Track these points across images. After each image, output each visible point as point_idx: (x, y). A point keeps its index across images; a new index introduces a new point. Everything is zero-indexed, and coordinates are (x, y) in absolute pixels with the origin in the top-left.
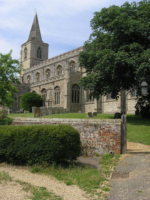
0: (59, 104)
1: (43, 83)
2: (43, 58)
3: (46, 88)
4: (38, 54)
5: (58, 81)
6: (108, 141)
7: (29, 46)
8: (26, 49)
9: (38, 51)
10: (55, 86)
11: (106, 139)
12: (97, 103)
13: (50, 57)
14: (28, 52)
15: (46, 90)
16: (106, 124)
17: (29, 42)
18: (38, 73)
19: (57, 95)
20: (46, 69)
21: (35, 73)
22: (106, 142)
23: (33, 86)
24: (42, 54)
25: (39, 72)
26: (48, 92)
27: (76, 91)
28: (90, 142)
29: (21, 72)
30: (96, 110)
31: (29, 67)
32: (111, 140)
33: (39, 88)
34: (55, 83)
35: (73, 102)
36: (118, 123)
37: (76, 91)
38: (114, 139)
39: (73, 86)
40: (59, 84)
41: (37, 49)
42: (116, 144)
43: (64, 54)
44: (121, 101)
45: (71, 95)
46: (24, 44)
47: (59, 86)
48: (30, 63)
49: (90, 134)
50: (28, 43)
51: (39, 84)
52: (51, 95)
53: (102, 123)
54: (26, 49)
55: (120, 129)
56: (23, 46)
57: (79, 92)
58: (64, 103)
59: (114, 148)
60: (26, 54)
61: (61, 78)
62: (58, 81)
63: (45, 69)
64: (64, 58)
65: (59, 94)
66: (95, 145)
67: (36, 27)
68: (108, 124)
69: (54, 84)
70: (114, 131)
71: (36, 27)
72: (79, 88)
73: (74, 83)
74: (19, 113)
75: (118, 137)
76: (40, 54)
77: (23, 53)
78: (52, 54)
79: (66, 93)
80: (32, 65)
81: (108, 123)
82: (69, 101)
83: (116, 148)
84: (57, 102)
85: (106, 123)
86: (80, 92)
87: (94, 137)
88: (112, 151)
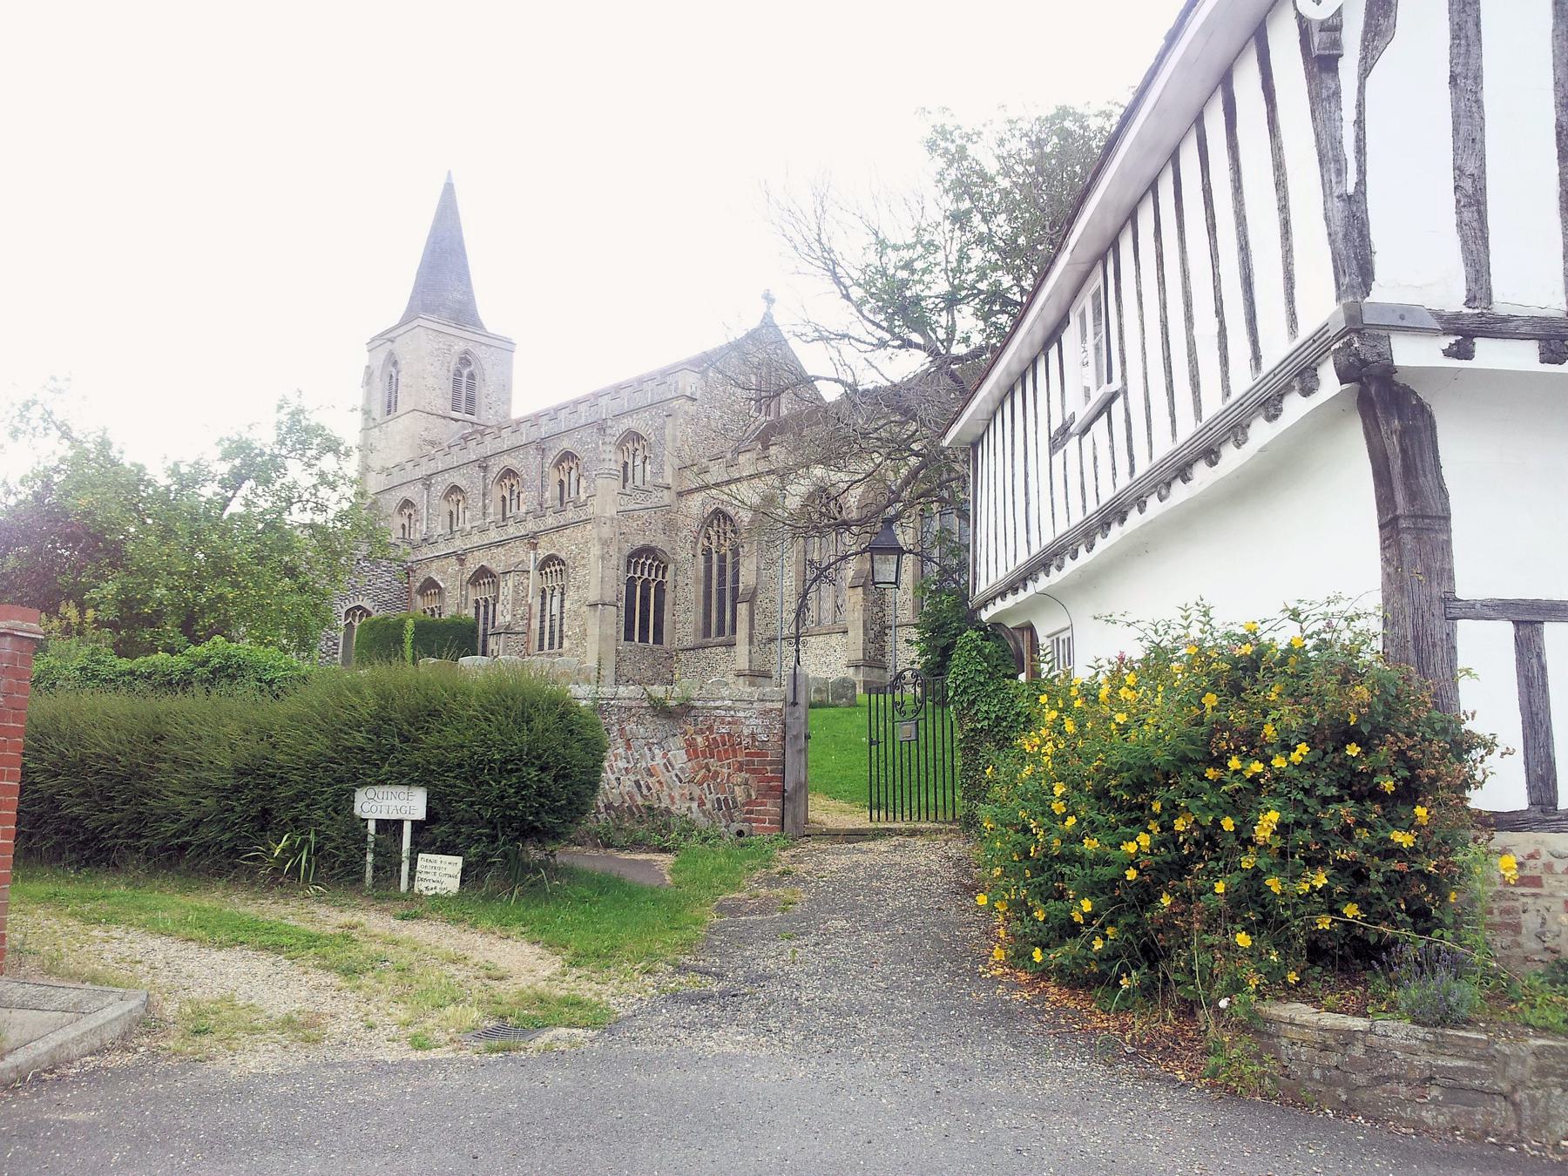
1: (476, 540)
3: (497, 568)
5: (559, 528)
9: (458, 373)
10: (542, 553)
11: (717, 773)
12: (751, 642)
15: (492, 575)
20: (496, 470)
21: (439, 488)
22: (720, 788)
24: (481, 393)
25: (462, 483)
26: (502, 584)
28: (649, 789)
29: (969, 220)
32: (739, 777)
35: (629, 637)
36: (769, 705)
38: (754, 771)
39: (631, 556)
40: (563, 545)
45: (622, 604)
47: (563, 555)
51: (458, 544)
54: (395, 363)
56: (378, 342)
57: (660, 587)
61: (570, 514)
62: (559, 528)
63: (496, 468)
64: (535, 434)
66: (672, 798)
67: (442, 284)
68: (730, 708)
69: (534, 546)
70: (753, 736)
71: (442, 284)
72: (665, 568)
73: (639, 542)
76: (471, 387)
81: (729, 703)
84: (552, 638)
85: (718, 703)
86: (668, 587)
87: (668, 766)
88: (744, 827)
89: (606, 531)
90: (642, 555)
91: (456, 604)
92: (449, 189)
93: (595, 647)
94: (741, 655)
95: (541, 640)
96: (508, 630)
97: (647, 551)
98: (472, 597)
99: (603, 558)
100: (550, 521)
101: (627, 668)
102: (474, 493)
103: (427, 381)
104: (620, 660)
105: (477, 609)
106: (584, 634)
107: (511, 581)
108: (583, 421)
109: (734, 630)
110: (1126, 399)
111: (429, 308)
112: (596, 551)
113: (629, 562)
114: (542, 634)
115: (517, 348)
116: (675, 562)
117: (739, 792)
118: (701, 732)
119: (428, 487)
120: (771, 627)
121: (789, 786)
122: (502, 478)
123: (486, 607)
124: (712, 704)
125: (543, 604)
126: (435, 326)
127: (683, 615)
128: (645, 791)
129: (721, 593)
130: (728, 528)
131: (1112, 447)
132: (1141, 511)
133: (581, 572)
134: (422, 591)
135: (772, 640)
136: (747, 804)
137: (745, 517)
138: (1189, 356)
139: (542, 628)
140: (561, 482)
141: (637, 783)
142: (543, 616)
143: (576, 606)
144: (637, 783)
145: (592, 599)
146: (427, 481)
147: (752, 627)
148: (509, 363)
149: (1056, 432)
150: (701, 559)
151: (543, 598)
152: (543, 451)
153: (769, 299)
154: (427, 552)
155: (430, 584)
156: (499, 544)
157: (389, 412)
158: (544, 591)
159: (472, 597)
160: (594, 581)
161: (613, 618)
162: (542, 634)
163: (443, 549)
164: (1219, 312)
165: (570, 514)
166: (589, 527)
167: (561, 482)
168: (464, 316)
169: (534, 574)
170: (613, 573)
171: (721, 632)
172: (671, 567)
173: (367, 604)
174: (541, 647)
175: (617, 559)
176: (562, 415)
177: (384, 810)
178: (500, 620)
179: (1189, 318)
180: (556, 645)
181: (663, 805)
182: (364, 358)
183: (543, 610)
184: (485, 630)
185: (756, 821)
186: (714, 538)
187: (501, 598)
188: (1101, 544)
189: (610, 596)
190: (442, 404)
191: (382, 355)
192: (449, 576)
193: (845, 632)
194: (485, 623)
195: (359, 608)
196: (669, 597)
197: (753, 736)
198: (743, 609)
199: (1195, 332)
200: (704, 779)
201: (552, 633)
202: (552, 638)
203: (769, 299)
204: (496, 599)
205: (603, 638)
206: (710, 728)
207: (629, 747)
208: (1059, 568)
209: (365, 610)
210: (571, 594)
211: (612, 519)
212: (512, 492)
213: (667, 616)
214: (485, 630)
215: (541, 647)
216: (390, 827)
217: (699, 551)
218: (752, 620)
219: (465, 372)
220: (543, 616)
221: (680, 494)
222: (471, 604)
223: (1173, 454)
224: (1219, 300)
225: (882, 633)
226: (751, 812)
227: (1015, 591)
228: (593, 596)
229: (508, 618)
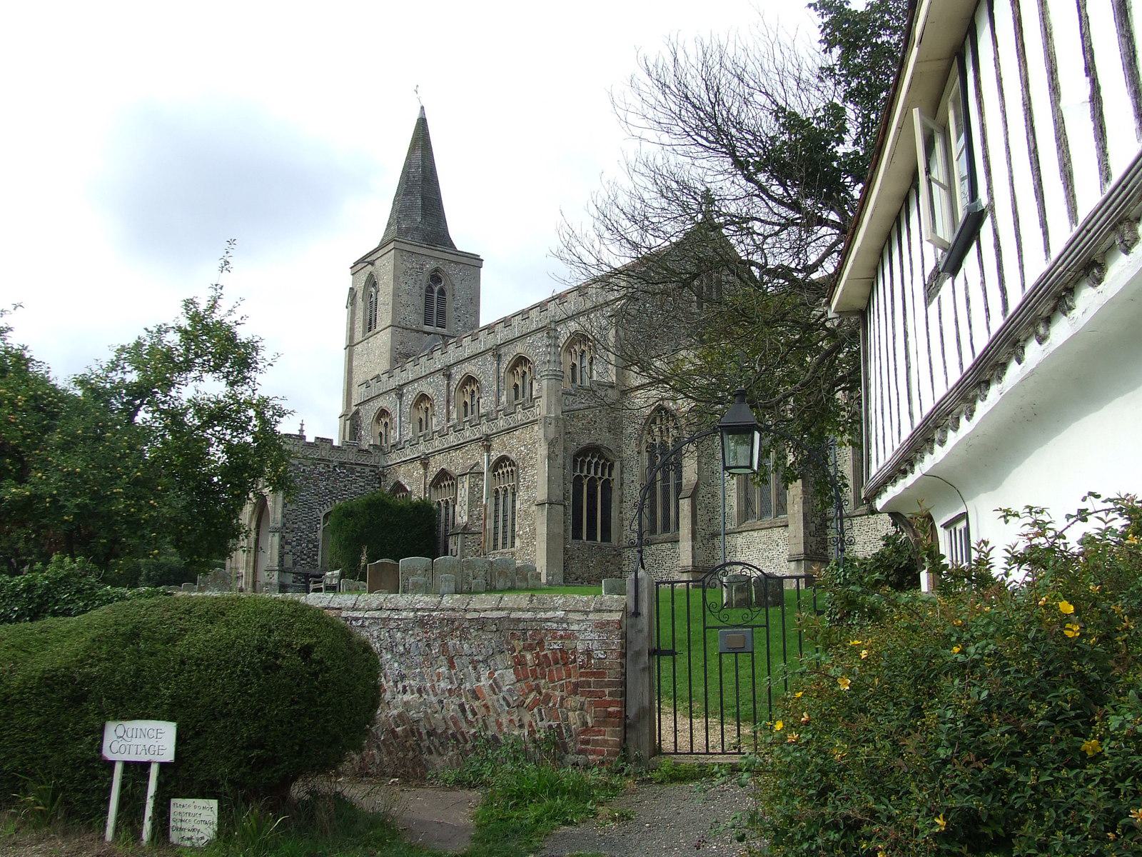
0: (513, 546)
1: (437, 444)
2: (452, 326)
4: (428, 300)
5: (509, 430)
6: (561, 706)
7: (386, 268)
8: (372, 282)
9: (430, 290)
10: (495, 455)
12: (694, 538)
13: (487, 317)
14: (380, 299)
16: (547, 620)
17: (386, 250)
18: (423, 397)
19: (504, 498)
20: (458, 377)
21: (410, 397)
22: (552, 713)
23: (395, 458)
25: (429, 391)
26: (460, 486)
27: (592, 482)
30: (685, 574)
31: (386, 366)
32: (573, 701)
33: (422, 471)
34: (496, 443)
35: (577, 535)
37: (592, 482)
39: (578, 455)
41: (425, 279)
42: (599, 723)
43: (542, 306)
44: (806, 527)
45: (569, 502)
46: (362, 260)
47: (513, 456)
48: (389, 347)
49: (475, 668)
50: (381, 252)
51: (422, 448)
52: (474, 501)
53: (529, 615)
54: (375, 284)
55: (616, 641)
56: (360, 266)
57: (607, 487)
58: (534, 544)
59: (587, 742)
60: (372, 307)
61: (520, 416)
62: (509, 430)
65: (514, 494)
66: (499, 725)
67: (420, 192)
68: (562, 621)
69: (488, 449)
70: (588, 653)
71: (420, 192)
73: (585, 441)
74: (319, 590)
75: (609, 684)
76: (442, 301)
77: (360, 303)
78: (499, 298)
79: (541, 493)
80: (400, 357)
81: (560, 614)
82: (559, 529)
83: (596, 743)
84: (505, 538)
85: (550, 614)
86: (615, 485)
87: (495, 687)
95: (496, 540)
96: (466, 530)
100: (501, 423)
101: (576, 566)
102: (439, 402)
104: (568, 558)
108: (534, 327)
110: (993, 217)
113: (575, 461)
114: (496, 534)
117: (574, 717)
118: (530, 648)
119: (400, 396)
121: (632, 712)
124: (542, 615)
125: (497, 505)
126: (408, 248)
128: (470, 716)
131: (983, 283)
132: (1019, 362)
136: (583, 732)
138: (1058, 139)
141: (462, 706)
142: (496, 516)
143: (526, 506)
144: (462, 706)
145: (1017, 518)
146: (399, 391)
147: (694, 522)
149: (930, 277)
150: (645, 455)
151: (497, 499)
152: (499, 357)
156: (457, 447)
157: (370, 330)
158: (497, 492)
164: (1090, 69)
165: (520, 416)
166: (536, 428)
172: (617, 465)
176: (515, 322)
177: (133, 749)
179: (1054, 89)
180: (509, 544)
181: (489, 733)
182: (347, 281)
183: (496, 511)
185: (594, 752)
187: (459, 499)
188: (982, 408)
191: (363, 277)
193: (787, 526)
197: (588, 653)
198: (685, 505)
199: (1062, 104)
200: (536, 703)
204: (455, 500)
206: (541, 643)
207: (451, 665)
208: (942, 443)
210: (522, 494)
213: (614, 514)
214: (446, 531)
216: (137, 770)
217: (644, 447)
219: (436, 289)
220: (496, 516)
223: (1046, 276)
224: (1088, 51)
226: (587, 742)
227: (904, 473)
229: (465, 519)
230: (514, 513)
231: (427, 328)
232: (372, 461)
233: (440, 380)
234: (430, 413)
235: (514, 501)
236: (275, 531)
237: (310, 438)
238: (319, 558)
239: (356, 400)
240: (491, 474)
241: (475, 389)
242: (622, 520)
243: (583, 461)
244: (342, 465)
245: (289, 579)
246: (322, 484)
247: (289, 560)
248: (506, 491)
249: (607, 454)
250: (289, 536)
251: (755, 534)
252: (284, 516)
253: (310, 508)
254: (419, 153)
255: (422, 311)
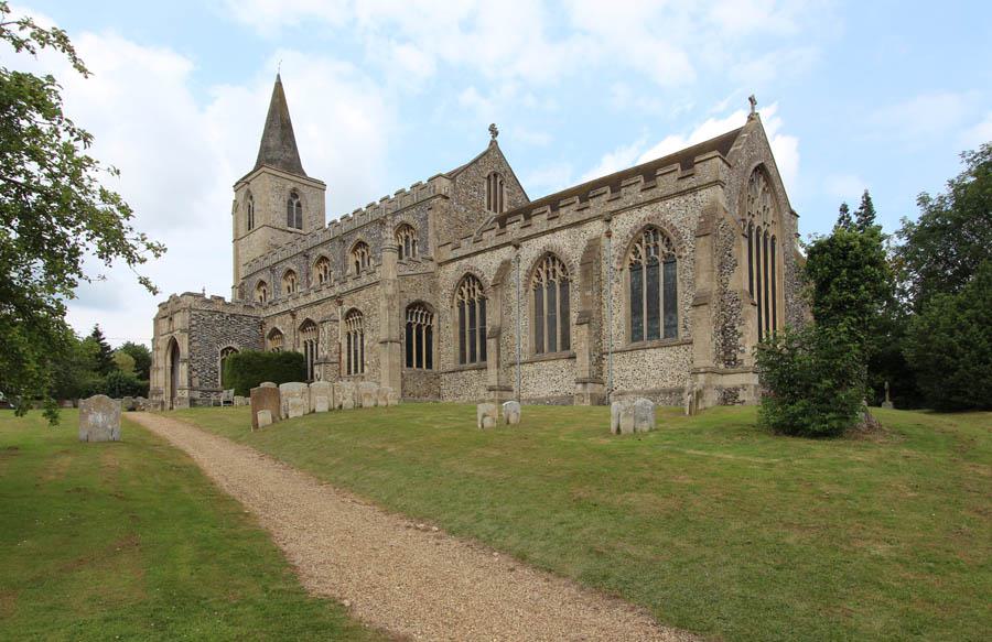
0: (362, 371)
1: (303, 301)
5: (357, 290)
9: (290, 203)
10: (346, 307)
12: (498, 366)
15: (314, 324)
21: (281, 272)
25: (294, 268)
27: (419, 328)
35: (409, 364)
37: (419, 328)
39: (408, 308)
40: (360, 301)
41: (287, 196)
47: (360, 308)
51: (292, 305)
54: (251, 197)
57: (429, 330)
61: (365, 279)
62: (357, 290)
65: (362, 336)
69: (341, 303)
72: (432, 316)
73: (414, 298)
76: (299, 212)
86: (434, 330)
89: (390, 290)
90: (415, 307)
91: (292, 343)
92: (279, 85)
93: (387, 371)
94: (492, 375)
95: (349, 367)
96: (326, 361)
97: (419, 304)
98: (302, 340)
99: (389, 309)
100: (351, 285)
101: (409, 386)
103: (271, 204)
105: (306, 347)
106: (378, 364)
107: (327, 327)
109: (484, 357)
111: (271, 162)
112: (383, 304)
113: (407, 312)
114: (349, 364)
115: (327, 188)
116: (439, 312)
119: (273, 271)
120: (512, 355)
122: (319, 262)
123: (312, 346)
127: (446, 349)
129: (473, 333)
130: (476, 287)
133: (374, 319)
134: (271, 337)
135: (512, 365)
137: (489, 279)
139: (349, 359)
140: (357, 262)
142: (349, 351)
145: (383, 338)
146: (272, 269)
148: (323, 198)
150: (457, 309)
153: (494, 131)
154: (272, 311)
155: (276, 331)
158: (349, 334)
159: (302, 340)
160: (384, 326)
161: (397, 353)
162: (349, 364)
163: (282, 308)
165: (365, 279)
166: (378, 287)
167: (357, 262)
168: (293, 165)
169: (342, 322)
170: (395, 319)
171: (473, 359)
173: (236, 346)
174: (349, 372)
175: (399, 310)
178: (320, 354)
183: (349, 347)
184: (312, 361)
186: (642, 252)
189: (395, 334)
190: (282, 222)
191: (242, 193)
192: (285, 325)
193: (575, 357)
194: (312, 357)
195: (230, 348)
196: (435, 337)
198: (491, 343)
201: (356, 351)
202: (356, 366)
203: (494, 131)
205: (392, 366)
209: (234, 350)
210: (368, 336)
211: (394, 281)
212: (326, 271)
213: (434, 350)
214: (312, 361)
215: (349, 372)
218: (498, 350)
219: (295, 202)
220: (349, 351)
221: (440, 264)
222: (302, 345)
225: (600, 358)
228: (383, 335)
229: (326, 353)
230: (362, 349)
231: (289, 229)
232: (254, 314)
233: (301, 259)
234: (366, 256)
235: (362, 340)
236: (185, 361)
237: (208, 297)
238: (219, 380)
239: (243, 275)
240: (344, 322)
241: (410, 235)
242: (440, 354)
243: (412, 312)
244: (233, 316)
245: (197, 395)
246: (218, 329)
247: (196, 382)
248: (356, 333)
249: (428, 307)
250: (195, 365)
251: (544, 364)
252: (190, 351)
253: (210, 346)
254: (277, 133)
255: (286, 216)
